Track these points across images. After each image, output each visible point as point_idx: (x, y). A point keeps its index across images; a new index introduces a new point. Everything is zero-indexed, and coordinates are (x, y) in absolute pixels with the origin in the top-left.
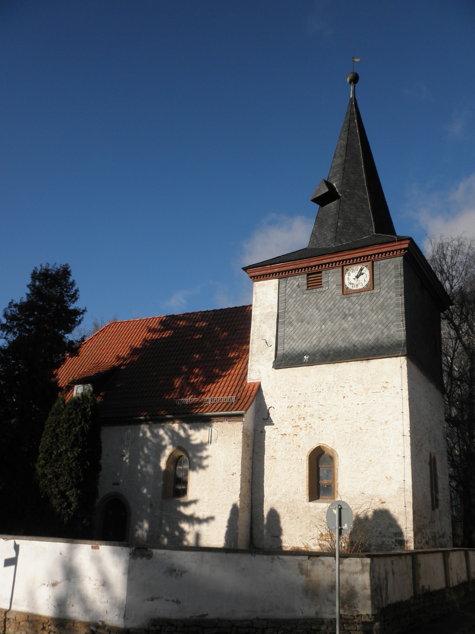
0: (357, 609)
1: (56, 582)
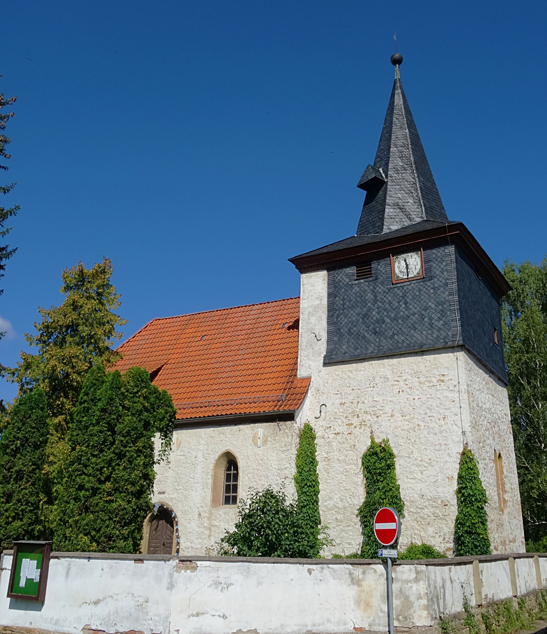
0: (412, 620)
1: (99, 599)
